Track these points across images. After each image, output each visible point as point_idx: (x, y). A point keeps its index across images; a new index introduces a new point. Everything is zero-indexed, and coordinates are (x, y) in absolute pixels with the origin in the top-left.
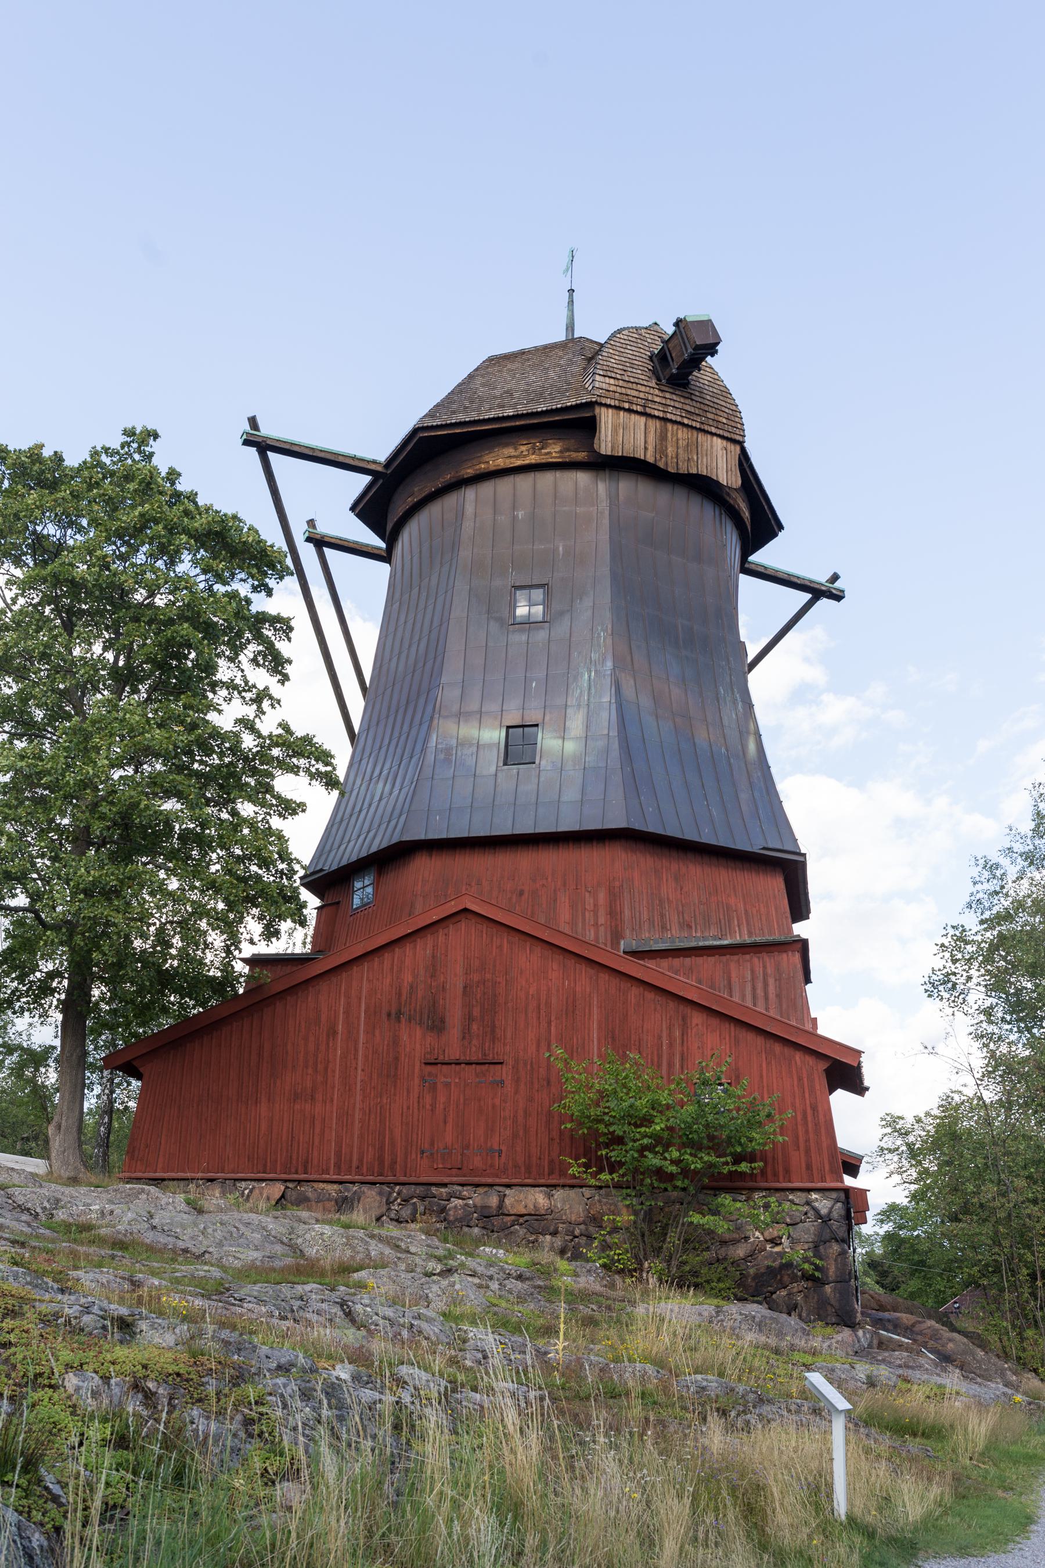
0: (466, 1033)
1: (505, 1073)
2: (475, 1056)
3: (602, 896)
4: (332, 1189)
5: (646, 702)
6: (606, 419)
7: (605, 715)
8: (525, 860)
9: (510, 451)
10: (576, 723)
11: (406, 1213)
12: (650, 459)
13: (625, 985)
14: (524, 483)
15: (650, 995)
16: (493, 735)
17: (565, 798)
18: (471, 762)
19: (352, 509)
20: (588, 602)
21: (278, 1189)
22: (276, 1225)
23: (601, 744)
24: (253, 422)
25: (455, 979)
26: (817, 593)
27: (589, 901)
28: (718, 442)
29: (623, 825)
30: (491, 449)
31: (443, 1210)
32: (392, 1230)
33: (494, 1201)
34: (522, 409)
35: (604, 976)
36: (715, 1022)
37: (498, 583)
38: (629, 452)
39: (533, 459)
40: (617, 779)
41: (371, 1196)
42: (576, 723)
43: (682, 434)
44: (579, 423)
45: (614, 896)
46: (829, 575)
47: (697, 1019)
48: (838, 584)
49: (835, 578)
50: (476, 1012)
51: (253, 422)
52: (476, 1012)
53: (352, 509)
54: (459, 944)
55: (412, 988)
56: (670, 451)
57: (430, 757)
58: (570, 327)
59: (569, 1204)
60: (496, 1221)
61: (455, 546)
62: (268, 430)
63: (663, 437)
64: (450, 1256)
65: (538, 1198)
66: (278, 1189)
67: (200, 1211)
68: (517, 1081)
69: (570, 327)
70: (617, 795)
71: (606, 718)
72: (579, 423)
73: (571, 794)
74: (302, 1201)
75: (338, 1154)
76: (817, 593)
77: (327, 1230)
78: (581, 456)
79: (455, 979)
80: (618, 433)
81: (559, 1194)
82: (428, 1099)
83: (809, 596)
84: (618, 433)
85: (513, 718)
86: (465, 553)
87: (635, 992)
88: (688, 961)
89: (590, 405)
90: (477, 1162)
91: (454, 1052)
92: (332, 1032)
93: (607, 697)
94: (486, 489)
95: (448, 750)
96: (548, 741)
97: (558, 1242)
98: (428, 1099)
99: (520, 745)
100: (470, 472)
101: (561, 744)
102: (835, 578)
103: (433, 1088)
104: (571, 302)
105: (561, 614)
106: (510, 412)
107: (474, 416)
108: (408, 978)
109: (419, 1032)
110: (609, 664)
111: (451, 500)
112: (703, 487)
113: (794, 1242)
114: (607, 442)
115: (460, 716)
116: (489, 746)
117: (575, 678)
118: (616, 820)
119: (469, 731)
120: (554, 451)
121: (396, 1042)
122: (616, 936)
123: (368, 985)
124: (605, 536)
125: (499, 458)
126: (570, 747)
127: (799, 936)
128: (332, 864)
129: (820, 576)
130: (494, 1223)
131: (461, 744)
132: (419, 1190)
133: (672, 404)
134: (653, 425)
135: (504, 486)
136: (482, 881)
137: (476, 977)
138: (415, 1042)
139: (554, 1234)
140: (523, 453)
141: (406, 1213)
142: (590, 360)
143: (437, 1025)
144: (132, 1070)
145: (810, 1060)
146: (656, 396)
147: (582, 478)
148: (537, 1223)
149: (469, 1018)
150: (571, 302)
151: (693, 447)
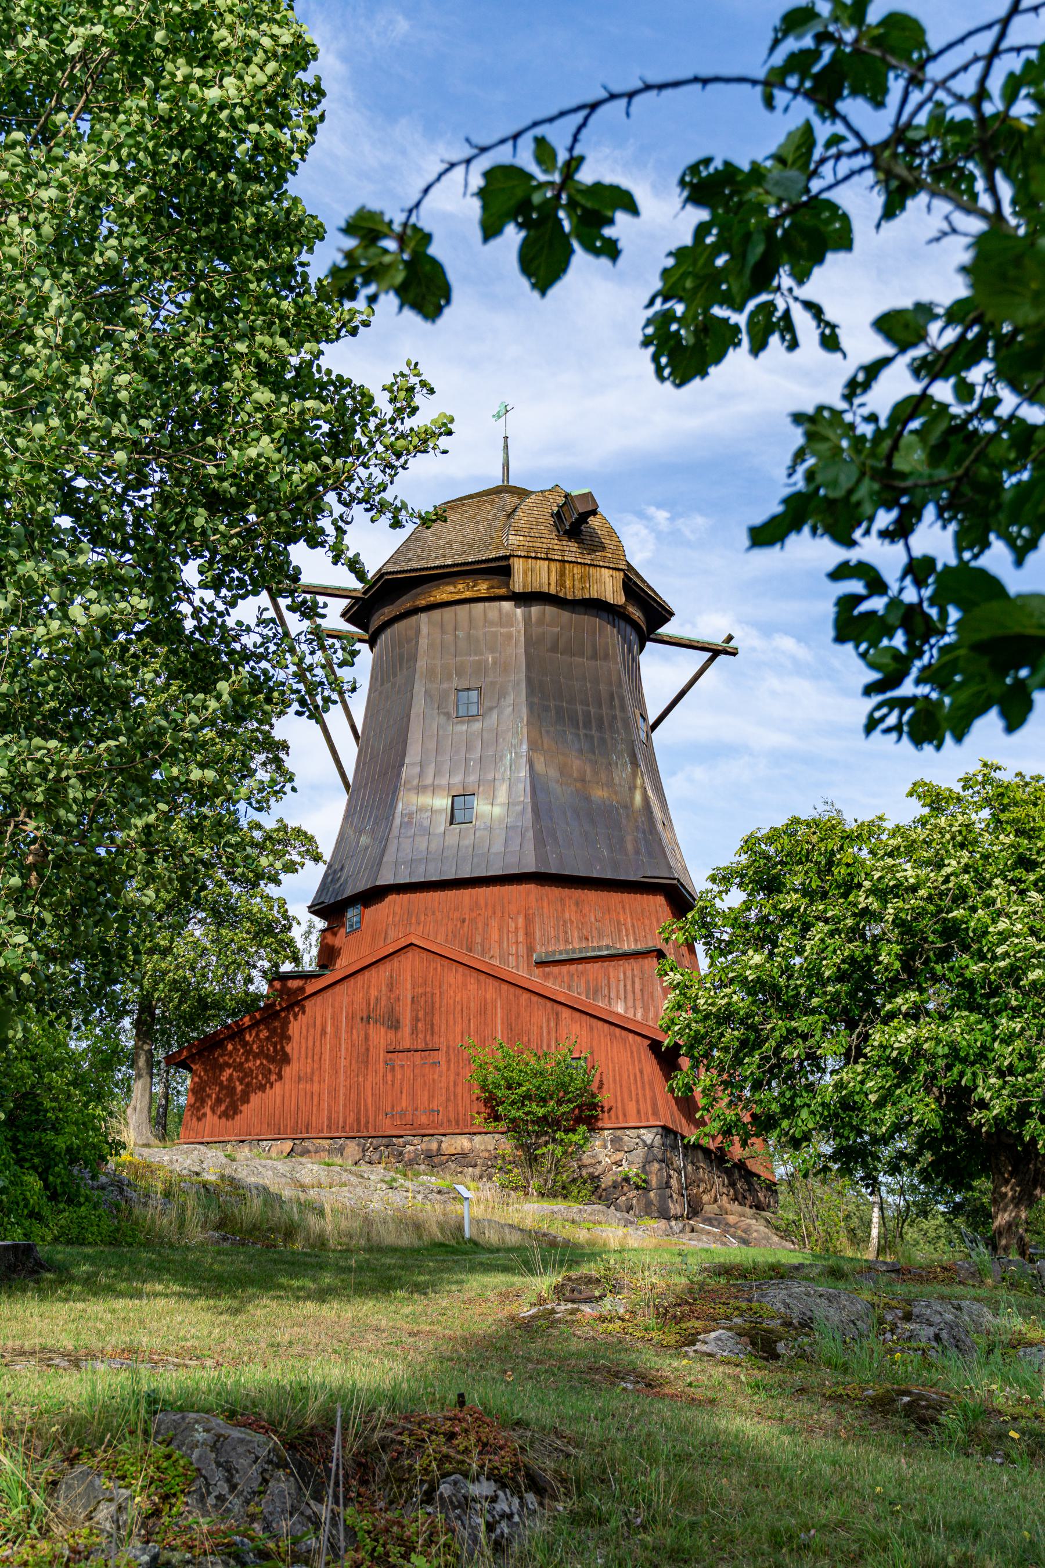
0: (414, 1031)
1: (441, 1056)
2: (421, 1046)
3: (521, 921)
4: (325, 1143)
5: (553, 773)
6: (518, 566)
7: (521, 786)
8: (466, 895)
10: (502, 795)
11: (375, 1157)
12: (553, 591)
13: (519, 991)
14: (462, 610)
15: (535, 998)
16: (442, 802)
17: (493, 850)
18: (426, 823)
19: (343, 615)
20: (510, 699)
21: (288, 1145)
22: (282, 1167)
23: (519, 808)
25: (406, 992)
26: (716, 652)
27: (512, 925)
28: (606, 572)
29: (533, 869)
30: (438, 587)
31: (401, 1154)
32: (364, 1167)
33: (434, 1146)
34: (458, 560)
35: (505, 986)
36: (577, 1015)
37: (445, 686)
39: (468, 594)
40: (530, 834)
41: (352, 1148)
42: (502, 795)
43: (577, 570)
44: (499, 569)
45: (529, 921)
46: (724, 637)
47: (566, 1013)
48: (732, 644)
49: (730, 638)
50: (421, 1015)
52: (421, 1015)
53: (343, 615)
54: (408, 966)
55: (377, 1000)
56: (568, 583)
57: (397, 821)
59: (482, 1144)
60: (436, 1160)
61: (414, 657)
63: (562, 574)
64: (394, 1180)
65: (463, 1143)
66: (288, 1145)
67: (233, 1160)
68: (448, 1061)
70: (530, 846)
71: (523, 789)
72: (499, 569)
73: (498, 847)
74: (305, 1152)
75: (329, 1118)
76: (716, 652)
77: (315, 1167)
78: (502, 591)
79: (406, 992)
80: (526, 575)
81: (477, 1139)
82: (389, 1077)
84: (526, 575)
86: (422, 664)
87: (526, 996)
88: (580, 967)
89: (506, 558)
90: (424, 1119)
91: (407, 1044)
92: (324, 1032)
93: (523, 773)
94: (436, 614)
95: (410, 815)
96: (481, 807)
97: (477, 1171)
98: (389, 1077)
100: (423, 603)
102: (730, 638)
103: (393, 1069)
104: (506, 447)
105: (491, 709)
106: (449, 562)
107: (424, 564)
108: (374, 993)
109: (383, 1030)
110: (525, 747)
111: (414, 618)
112: (596, 606)
113: (630, 1163)
114: (518, 584)
115: (420, 789)
116: (440, 811)
117: (501, 759)
118: (530, 866)
119: (425, 800)
120: (483, 587)
121: (367, 1038)
123: (346, 1000)
124: (522, 650)
125: (444, 593)
126: (497, 811)
128: (329, 900)
129: (717, 639)
130: (434, 1160)
131: (421, 809)
132: (385, 1141)
133: (571, 550)
134: (555, 566)
135: (448, 613)
136: (431, 920)
137: (420, 991)
138: (380, 1037)
139: (475, 1166)
141: (375, 1157)
142: (509, 516)
143: (395, 1025)
144: (184, 1065)
145: (638, 1039)
146: (556, 544)
147: (507, 605)
148: (463, 1158)
149: (416, 1019)
150: (506, 447)
151: (585, 578)
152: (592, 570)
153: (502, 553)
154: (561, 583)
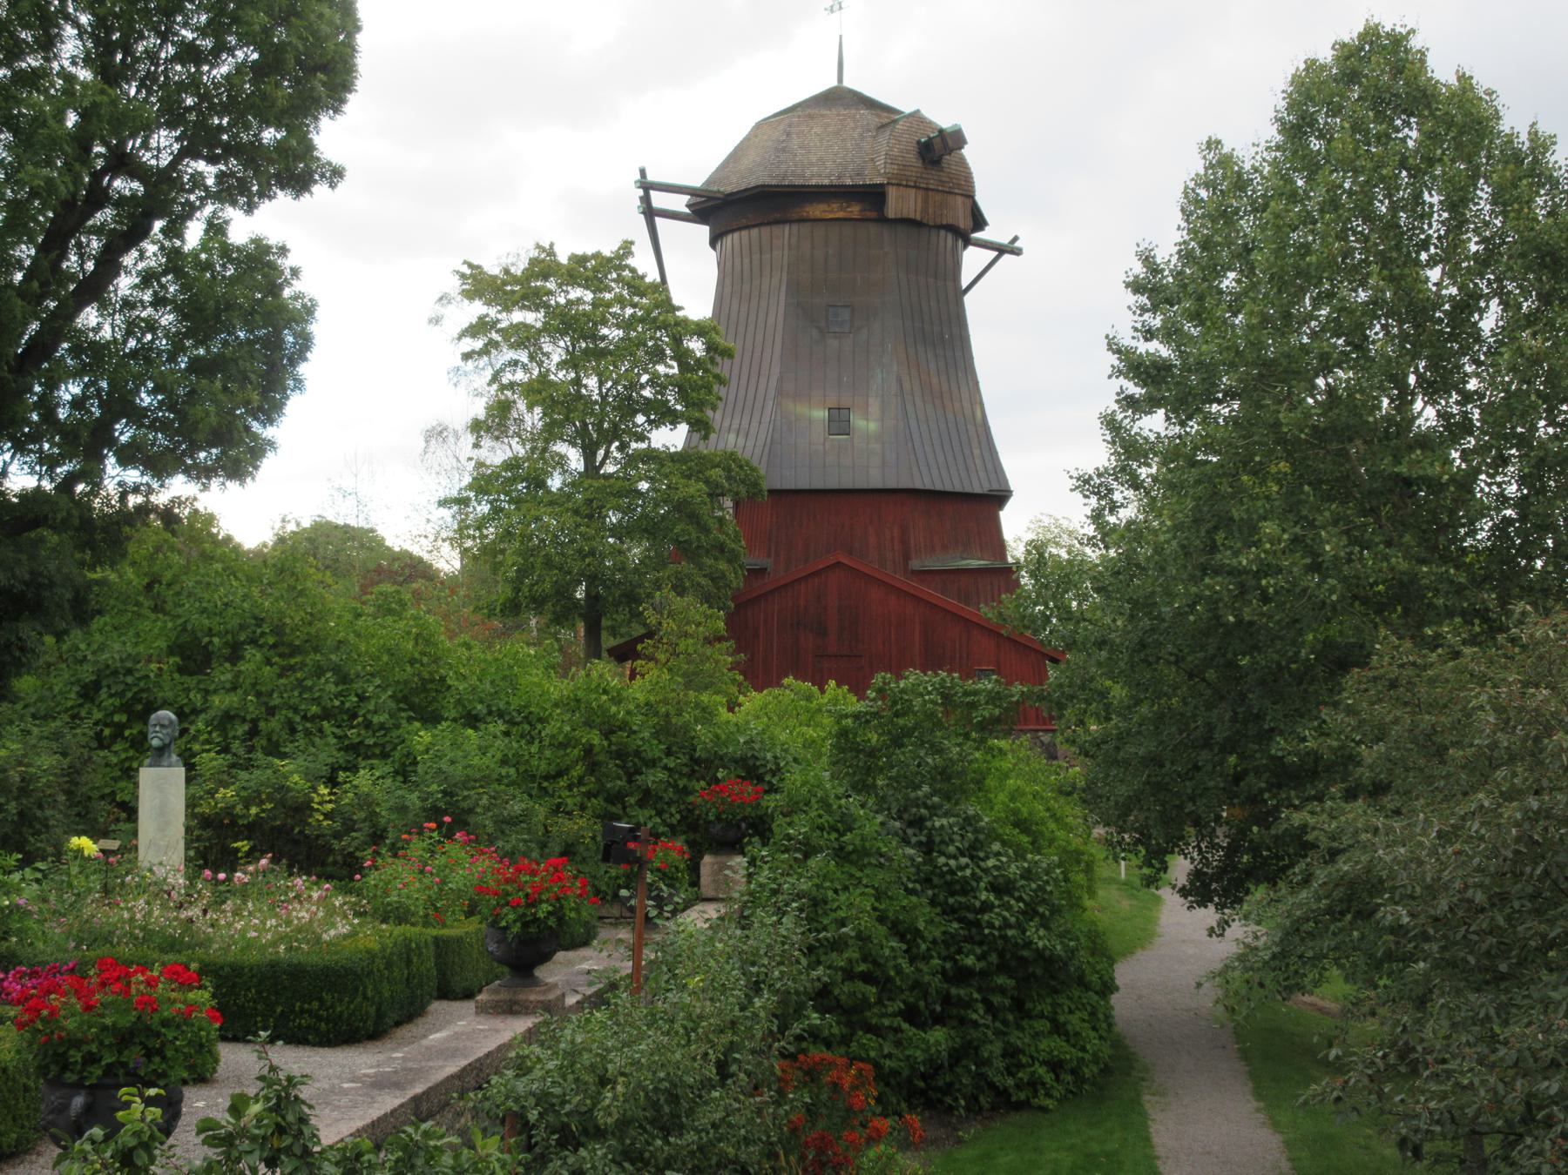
6: (892, 193)
9: (823, 207)
16: (821, 414)
24: (643, 172)
26: (1001, 250)
38: (905, 215)
39: (841, 215)
43: (938, 197)
48: (1017, 244)
49: (1016, 239)
51: (643, 172)
56: (931, 211)
58: (840, 79)
62: (651, 177)
63: (925, 201)
69: (840, 79)
72: (873, 196)
76: (1001, 250)
78: (873, 215)
83: (995, 253)
85: (832, 403)
89: (882, 185)
96: (858, 422)
99: (839, 422)
100: (795, 216)
101: (866, 424)
102: (1016, 239)
120: (855, 210)
122: (907, 558)
125: (817, 210)
127: (229, 539)
134: (920, 193)
140: (834, 210)
147: (873, 229)
152: (950, 198)
153: (878, 181)
154: (925, 210)
